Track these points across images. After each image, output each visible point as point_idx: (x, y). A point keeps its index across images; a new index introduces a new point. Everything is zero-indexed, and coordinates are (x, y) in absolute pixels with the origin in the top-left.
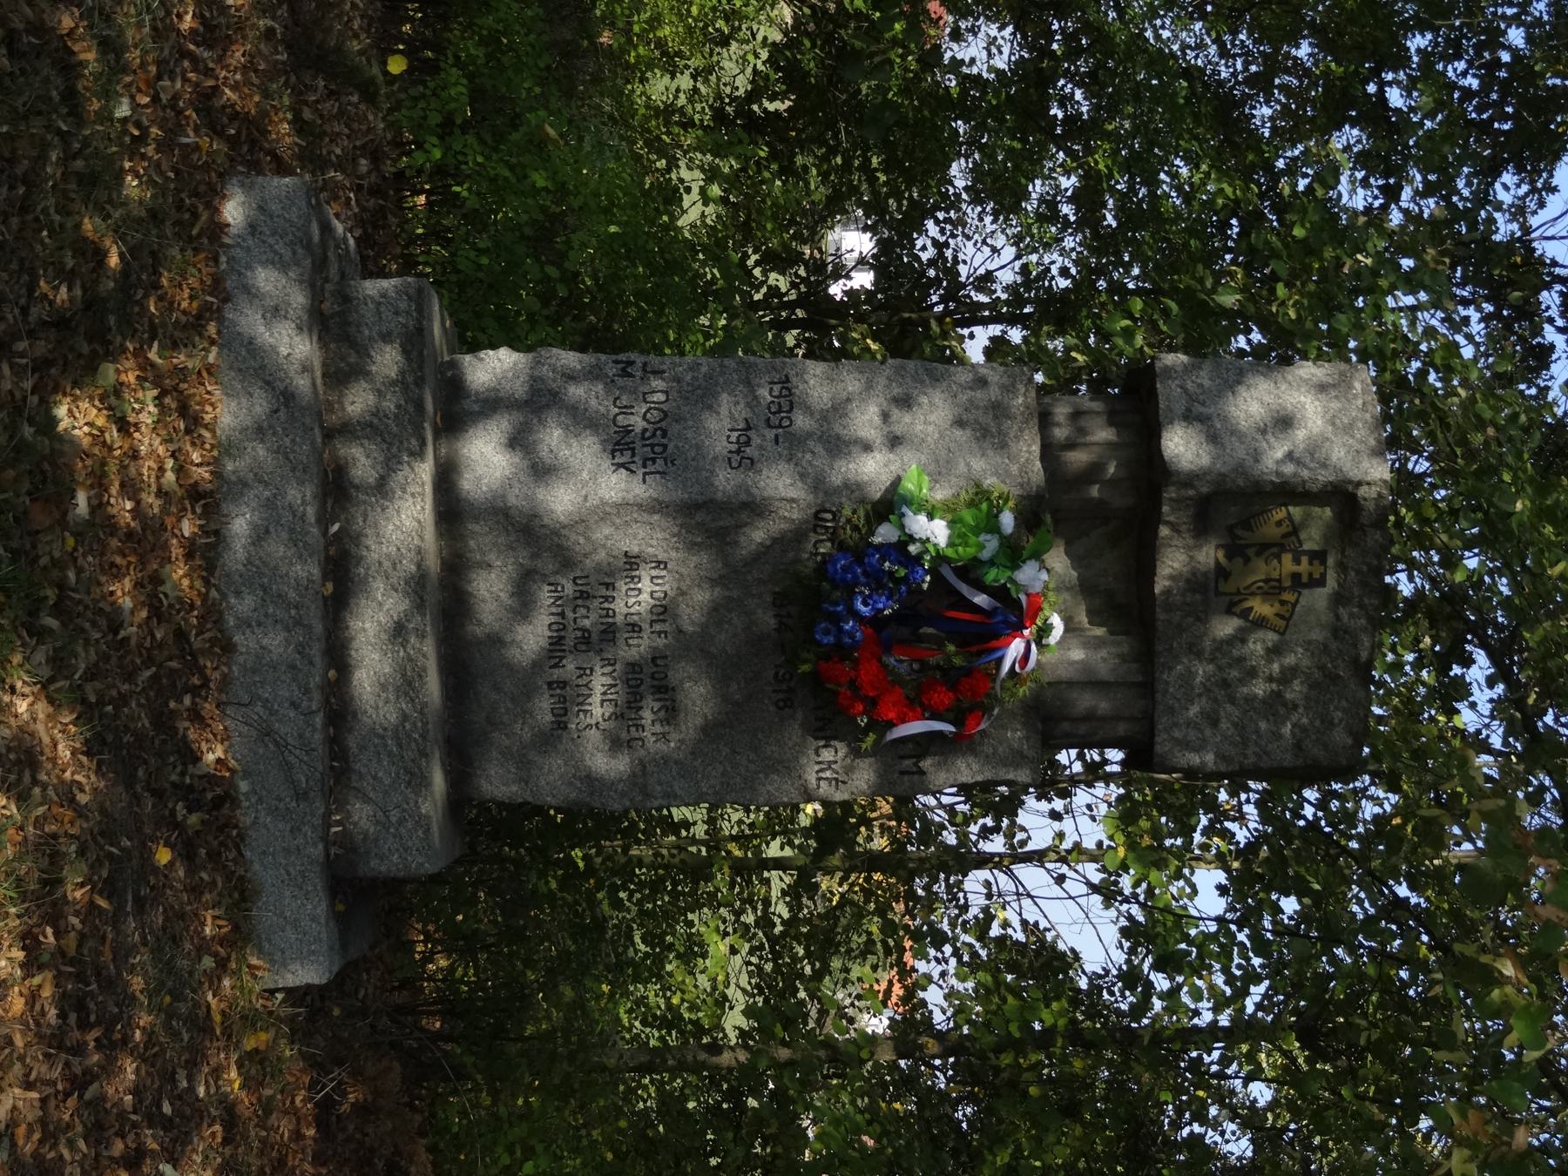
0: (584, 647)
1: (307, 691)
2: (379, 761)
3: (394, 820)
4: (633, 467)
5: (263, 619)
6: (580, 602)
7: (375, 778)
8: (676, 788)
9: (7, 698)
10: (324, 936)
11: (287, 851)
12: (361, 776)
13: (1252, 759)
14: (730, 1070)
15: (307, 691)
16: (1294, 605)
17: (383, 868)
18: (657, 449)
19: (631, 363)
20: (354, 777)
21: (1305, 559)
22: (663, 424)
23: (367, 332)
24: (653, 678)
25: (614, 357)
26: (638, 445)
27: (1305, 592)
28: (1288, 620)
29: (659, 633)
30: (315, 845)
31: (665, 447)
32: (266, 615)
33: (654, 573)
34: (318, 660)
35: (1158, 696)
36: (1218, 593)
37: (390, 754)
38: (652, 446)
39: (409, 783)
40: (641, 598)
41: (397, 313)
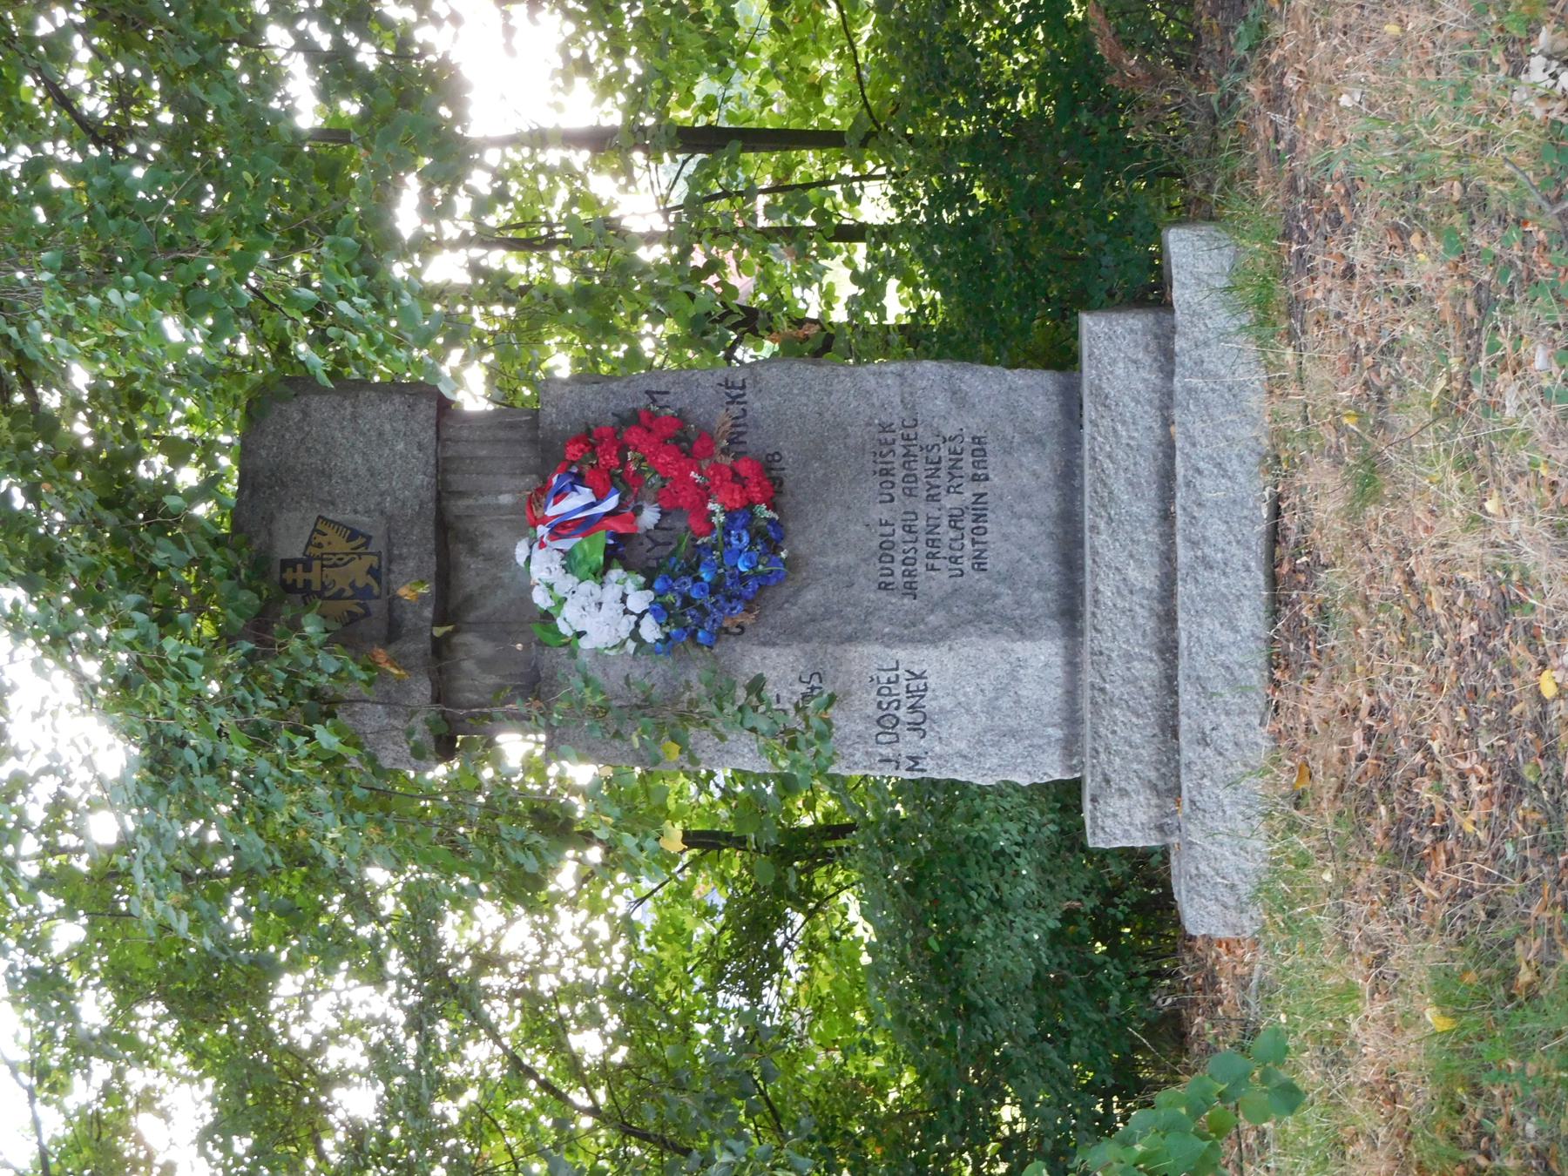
0: (956, 512)
1: (1188, 484)
2: (1133, 417)
3: (1121, 365)
4: (908, 676)
5: (1227, 547)
6: (959, 554)
7: (1138, 402)
8: (873, 382)
9: (157, 1170)
10: (1174, 271)
11: (1206, 344)
12: (1150, 402)
13: (347, 403)
14: (800, 322)
15: (1188, 484)
16: (309, 544)
17: (1131, 321)
18: (885, 691)
19: (910, 769)
20: (1157, 402)
21: (300, 585)
22: (881, 713)
23: (1141, 798)
24: (893, 484)
25: (924, 775)
26: (903, 696)
27: (299, 555)
28: (315, 530)
29: (887, 524)
30: (1182, 349)
31: (879, 693)
32: (1223, 551)
33: (890, 579)
34: (1179, 512)
35: (433, 461)
36: (379, 554)
37: (1124, 423)
38: (890, 694)
39: (1106, 397)
40: (902, 557)
41: (1115, 815)
